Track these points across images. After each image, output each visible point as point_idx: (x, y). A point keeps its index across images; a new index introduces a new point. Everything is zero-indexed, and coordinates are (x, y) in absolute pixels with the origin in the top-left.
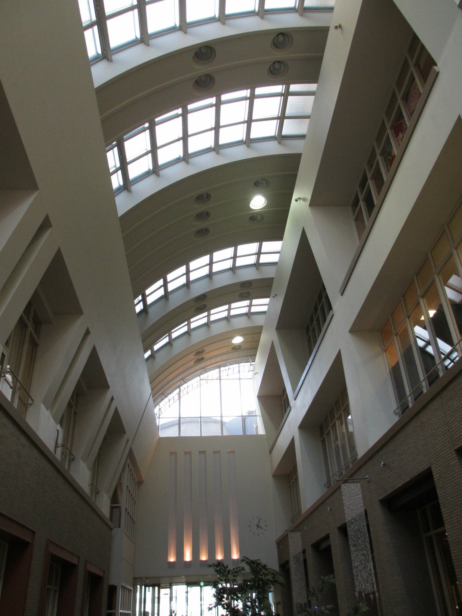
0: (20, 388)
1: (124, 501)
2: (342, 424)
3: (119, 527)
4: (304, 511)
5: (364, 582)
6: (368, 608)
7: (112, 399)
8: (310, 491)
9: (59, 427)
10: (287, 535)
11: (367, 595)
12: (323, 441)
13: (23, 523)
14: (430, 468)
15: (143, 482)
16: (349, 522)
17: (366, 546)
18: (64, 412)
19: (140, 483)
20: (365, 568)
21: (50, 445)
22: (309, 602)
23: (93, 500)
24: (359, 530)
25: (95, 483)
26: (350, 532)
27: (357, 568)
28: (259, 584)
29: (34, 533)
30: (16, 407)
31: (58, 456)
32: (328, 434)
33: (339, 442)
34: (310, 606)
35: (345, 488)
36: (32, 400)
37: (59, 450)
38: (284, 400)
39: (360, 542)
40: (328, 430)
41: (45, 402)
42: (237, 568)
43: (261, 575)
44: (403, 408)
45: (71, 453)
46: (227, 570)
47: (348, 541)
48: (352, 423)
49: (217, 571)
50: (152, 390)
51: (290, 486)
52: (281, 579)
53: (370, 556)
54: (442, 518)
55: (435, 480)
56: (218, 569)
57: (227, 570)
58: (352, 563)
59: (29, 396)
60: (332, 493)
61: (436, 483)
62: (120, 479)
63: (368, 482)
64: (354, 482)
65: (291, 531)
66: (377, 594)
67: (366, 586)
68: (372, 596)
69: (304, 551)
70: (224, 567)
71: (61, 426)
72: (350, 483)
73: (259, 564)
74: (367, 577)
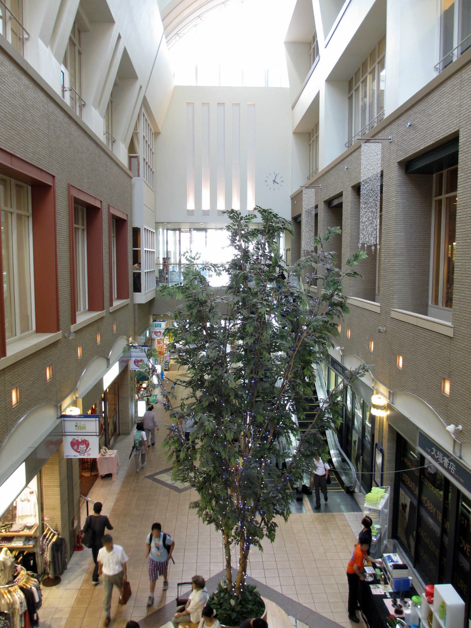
0: (10, 18)
1: (141, 151)
2: (373, 79)
3: (139, 176)
4: (320, 170)
5: (368, 235)
6: (367, 256)
7: (119, 37)
8: (329, 149)
9: (63, 68)
10: (302, 191)
11: (369, 247)
12: (350, 98)
13: (12, 152)
14: (458, 131)
15: (159, 133)
16: (363, 181)
17: (376, 205)
18: (67, 48)
19: (157, 134)
20: (371, 223)
21: (57, 90)
22: (316, 248)
23: (110, 148)
24: (372, 189)
25: (110, 132)
26: (363, 191)
27: (364, 223)
28: (269, 231)
29: (54, 177)
30: (10, 42)
31: (67, 100)
32: (357, 90)
33: (367, 100)
34: (316, 252)
35: (365, 147)
36: (28, 34)
37: (67, 94)
38: (314, 49)
39: (371, 200)
40: (357, 86)
41: (42, 37)
42: (249, 215)
43: (272, 222)
44: (447, 62)
45: (80, 99)
46: (240, 216)
47: (360, 199)
48: (385, 81)
49: (230, 217)
50: (165, 29)
51: (310, 145)
52: (290, 227)
53: (379, 214)
54: (457, 183)
55: (460, 144)
56: (231, 215)
57: (240, 216)
58: (359, 219)
59: (23, 29)
60: (353, 150)
61: (460, 147)
62: (136, 128)
63: (391, 142)
64: (376, 142)
65: (307, 187)
66: (378, 247)
67: (369, 239)
68: (373, 248)
69: (316, 207)
70: (237, 214)
71: (66, 66)
72: (372, 142)
73: (271, 213)
74: (372, 232)
